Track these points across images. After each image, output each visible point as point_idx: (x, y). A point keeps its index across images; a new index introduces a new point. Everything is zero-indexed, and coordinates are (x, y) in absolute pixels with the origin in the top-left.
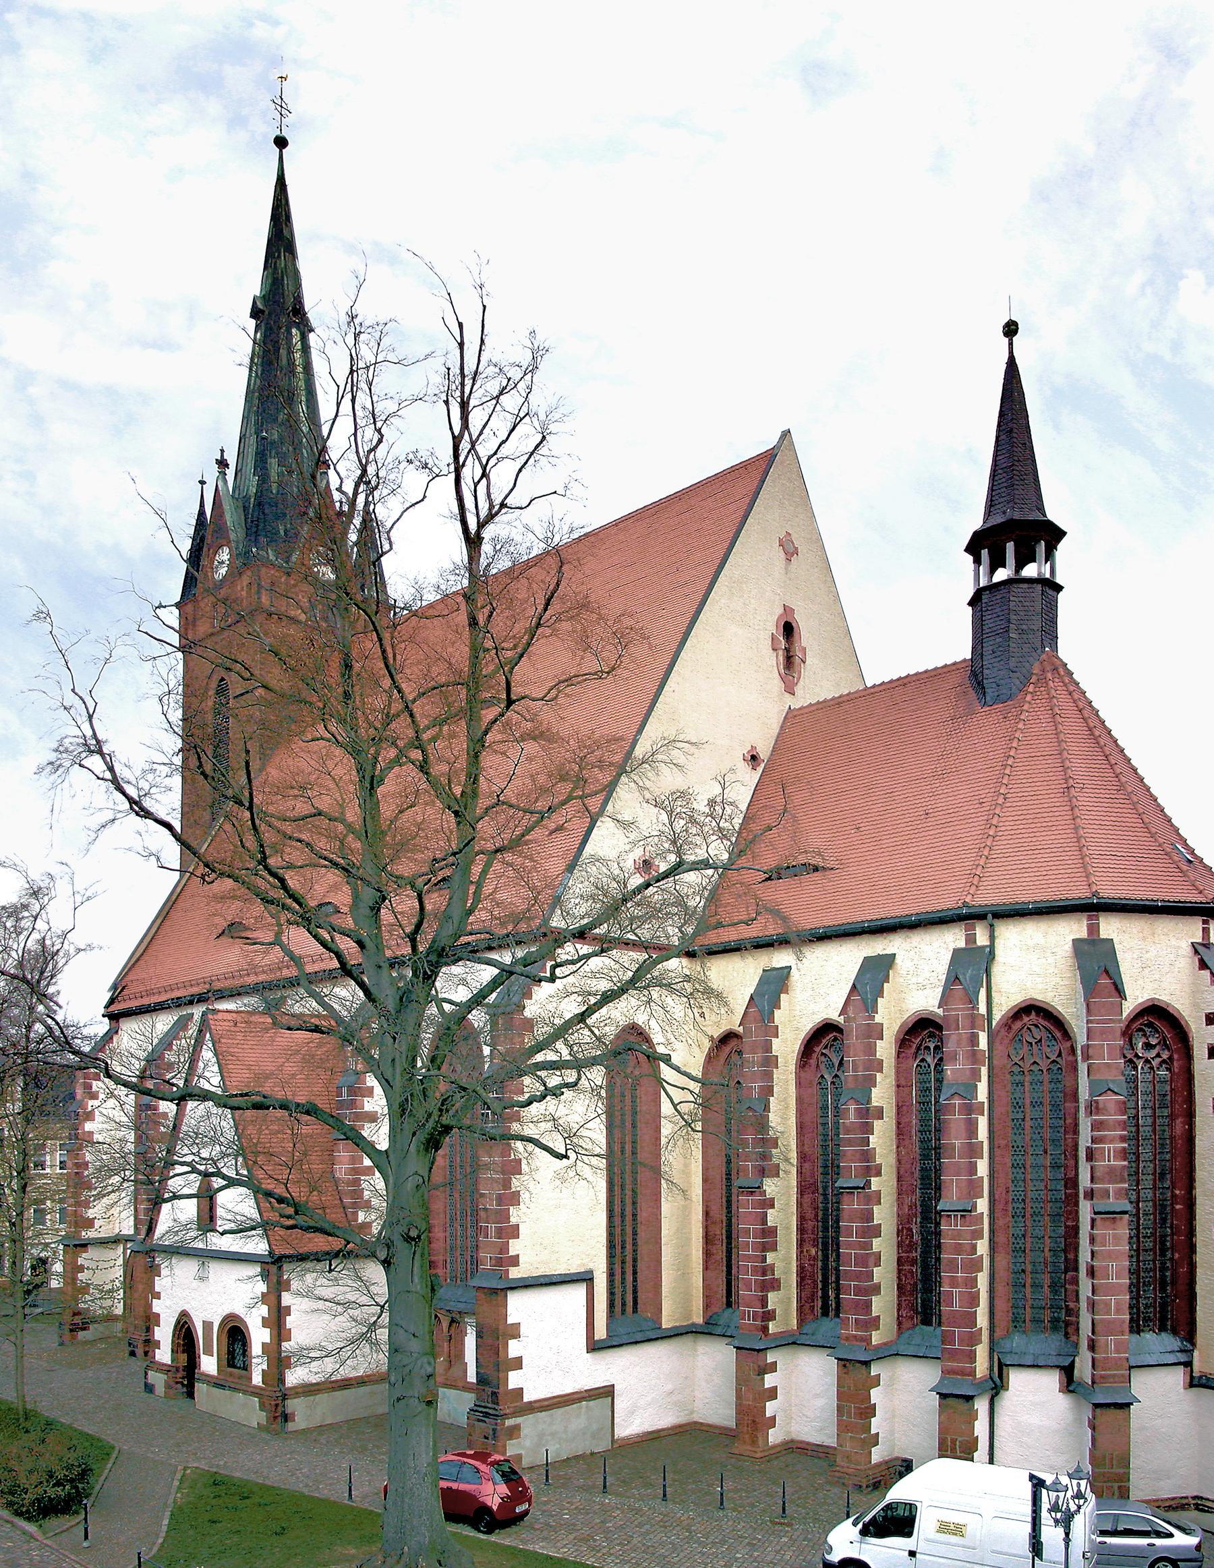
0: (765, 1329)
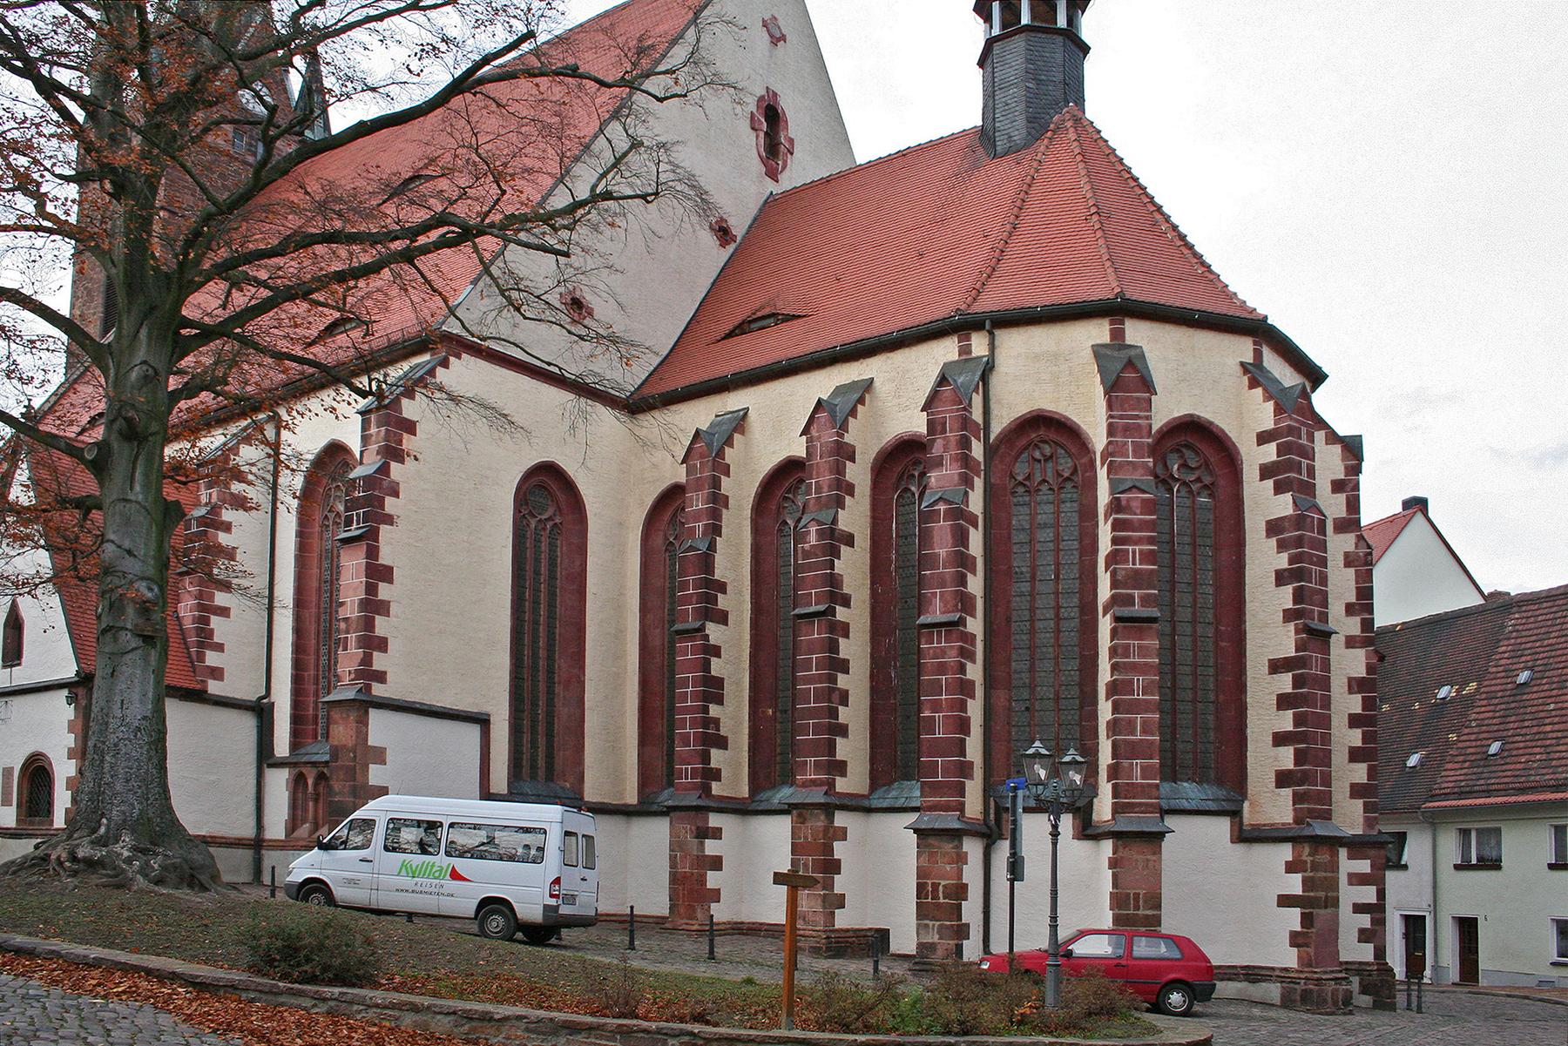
0: (706, 790)
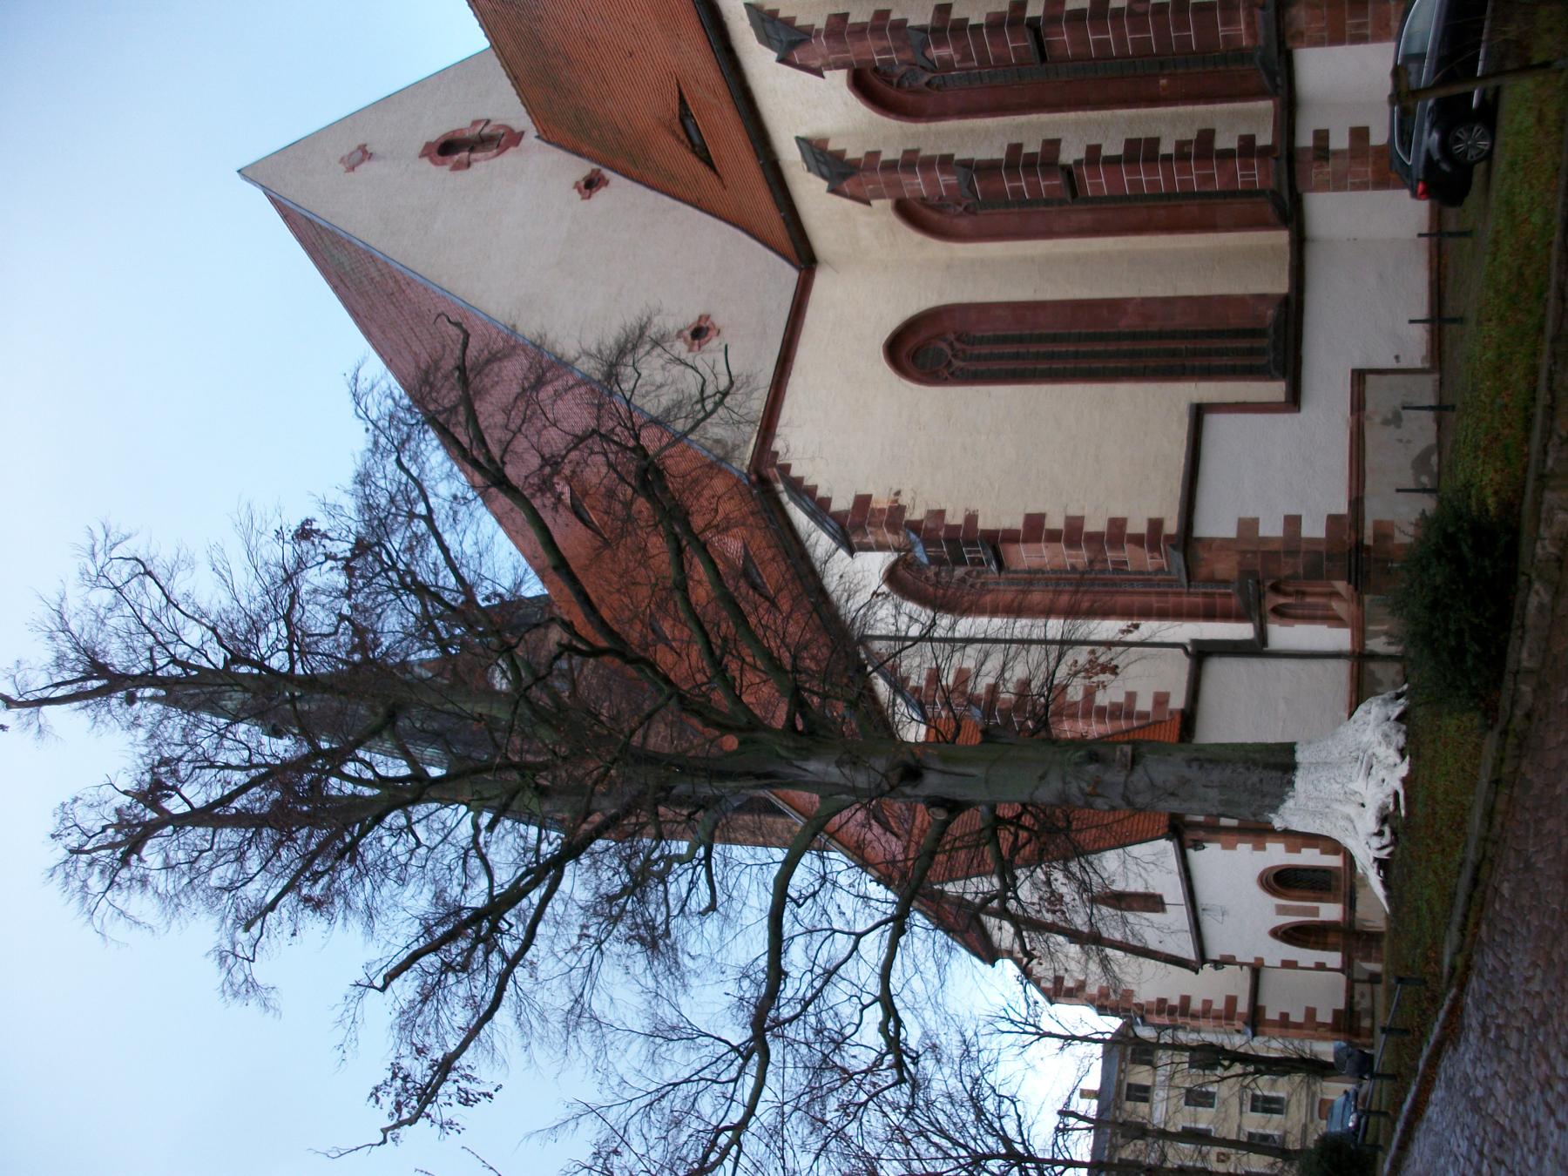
0: (1266, 151)
